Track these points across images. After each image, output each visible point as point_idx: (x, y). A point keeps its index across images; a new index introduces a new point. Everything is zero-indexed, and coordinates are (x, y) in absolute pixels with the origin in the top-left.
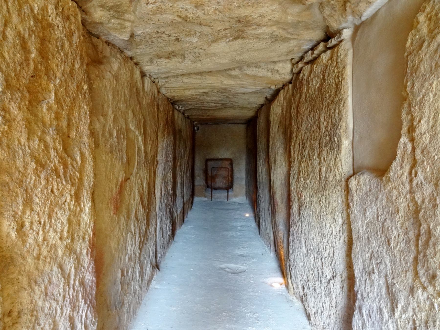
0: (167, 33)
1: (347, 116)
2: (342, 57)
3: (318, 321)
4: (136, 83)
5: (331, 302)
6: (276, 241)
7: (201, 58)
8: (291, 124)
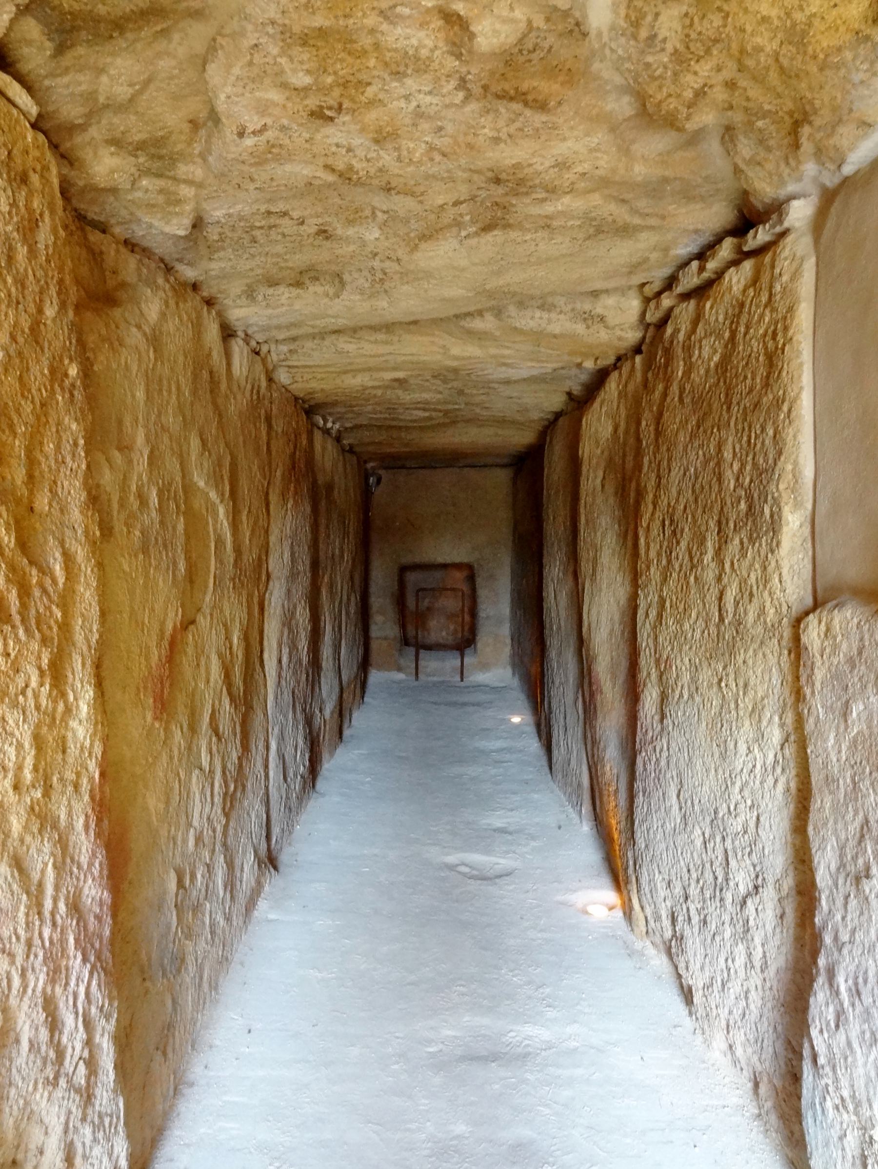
0: (295, 214)
1: (797, 446)
2: (785, 278)
3: (713, 1007)
4: (209, 355)
5: (750, 955)
6: (597, 794)
7: (387, 285)
8: (638, 467)
